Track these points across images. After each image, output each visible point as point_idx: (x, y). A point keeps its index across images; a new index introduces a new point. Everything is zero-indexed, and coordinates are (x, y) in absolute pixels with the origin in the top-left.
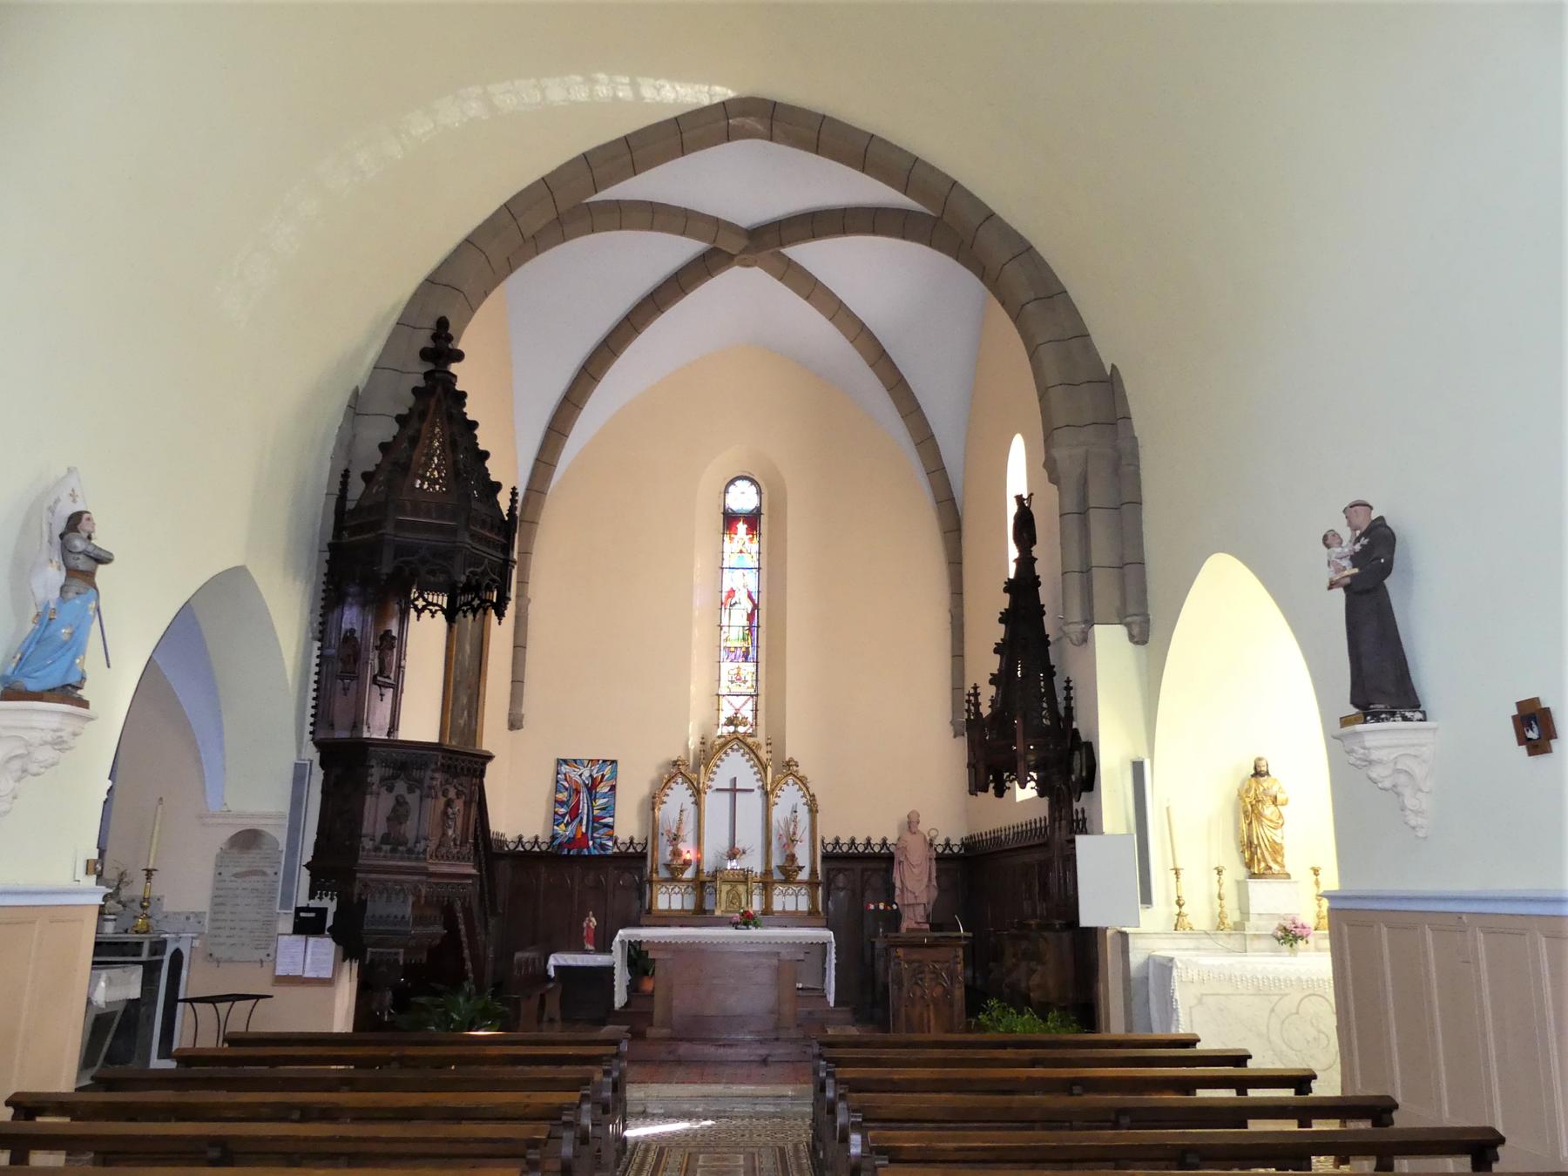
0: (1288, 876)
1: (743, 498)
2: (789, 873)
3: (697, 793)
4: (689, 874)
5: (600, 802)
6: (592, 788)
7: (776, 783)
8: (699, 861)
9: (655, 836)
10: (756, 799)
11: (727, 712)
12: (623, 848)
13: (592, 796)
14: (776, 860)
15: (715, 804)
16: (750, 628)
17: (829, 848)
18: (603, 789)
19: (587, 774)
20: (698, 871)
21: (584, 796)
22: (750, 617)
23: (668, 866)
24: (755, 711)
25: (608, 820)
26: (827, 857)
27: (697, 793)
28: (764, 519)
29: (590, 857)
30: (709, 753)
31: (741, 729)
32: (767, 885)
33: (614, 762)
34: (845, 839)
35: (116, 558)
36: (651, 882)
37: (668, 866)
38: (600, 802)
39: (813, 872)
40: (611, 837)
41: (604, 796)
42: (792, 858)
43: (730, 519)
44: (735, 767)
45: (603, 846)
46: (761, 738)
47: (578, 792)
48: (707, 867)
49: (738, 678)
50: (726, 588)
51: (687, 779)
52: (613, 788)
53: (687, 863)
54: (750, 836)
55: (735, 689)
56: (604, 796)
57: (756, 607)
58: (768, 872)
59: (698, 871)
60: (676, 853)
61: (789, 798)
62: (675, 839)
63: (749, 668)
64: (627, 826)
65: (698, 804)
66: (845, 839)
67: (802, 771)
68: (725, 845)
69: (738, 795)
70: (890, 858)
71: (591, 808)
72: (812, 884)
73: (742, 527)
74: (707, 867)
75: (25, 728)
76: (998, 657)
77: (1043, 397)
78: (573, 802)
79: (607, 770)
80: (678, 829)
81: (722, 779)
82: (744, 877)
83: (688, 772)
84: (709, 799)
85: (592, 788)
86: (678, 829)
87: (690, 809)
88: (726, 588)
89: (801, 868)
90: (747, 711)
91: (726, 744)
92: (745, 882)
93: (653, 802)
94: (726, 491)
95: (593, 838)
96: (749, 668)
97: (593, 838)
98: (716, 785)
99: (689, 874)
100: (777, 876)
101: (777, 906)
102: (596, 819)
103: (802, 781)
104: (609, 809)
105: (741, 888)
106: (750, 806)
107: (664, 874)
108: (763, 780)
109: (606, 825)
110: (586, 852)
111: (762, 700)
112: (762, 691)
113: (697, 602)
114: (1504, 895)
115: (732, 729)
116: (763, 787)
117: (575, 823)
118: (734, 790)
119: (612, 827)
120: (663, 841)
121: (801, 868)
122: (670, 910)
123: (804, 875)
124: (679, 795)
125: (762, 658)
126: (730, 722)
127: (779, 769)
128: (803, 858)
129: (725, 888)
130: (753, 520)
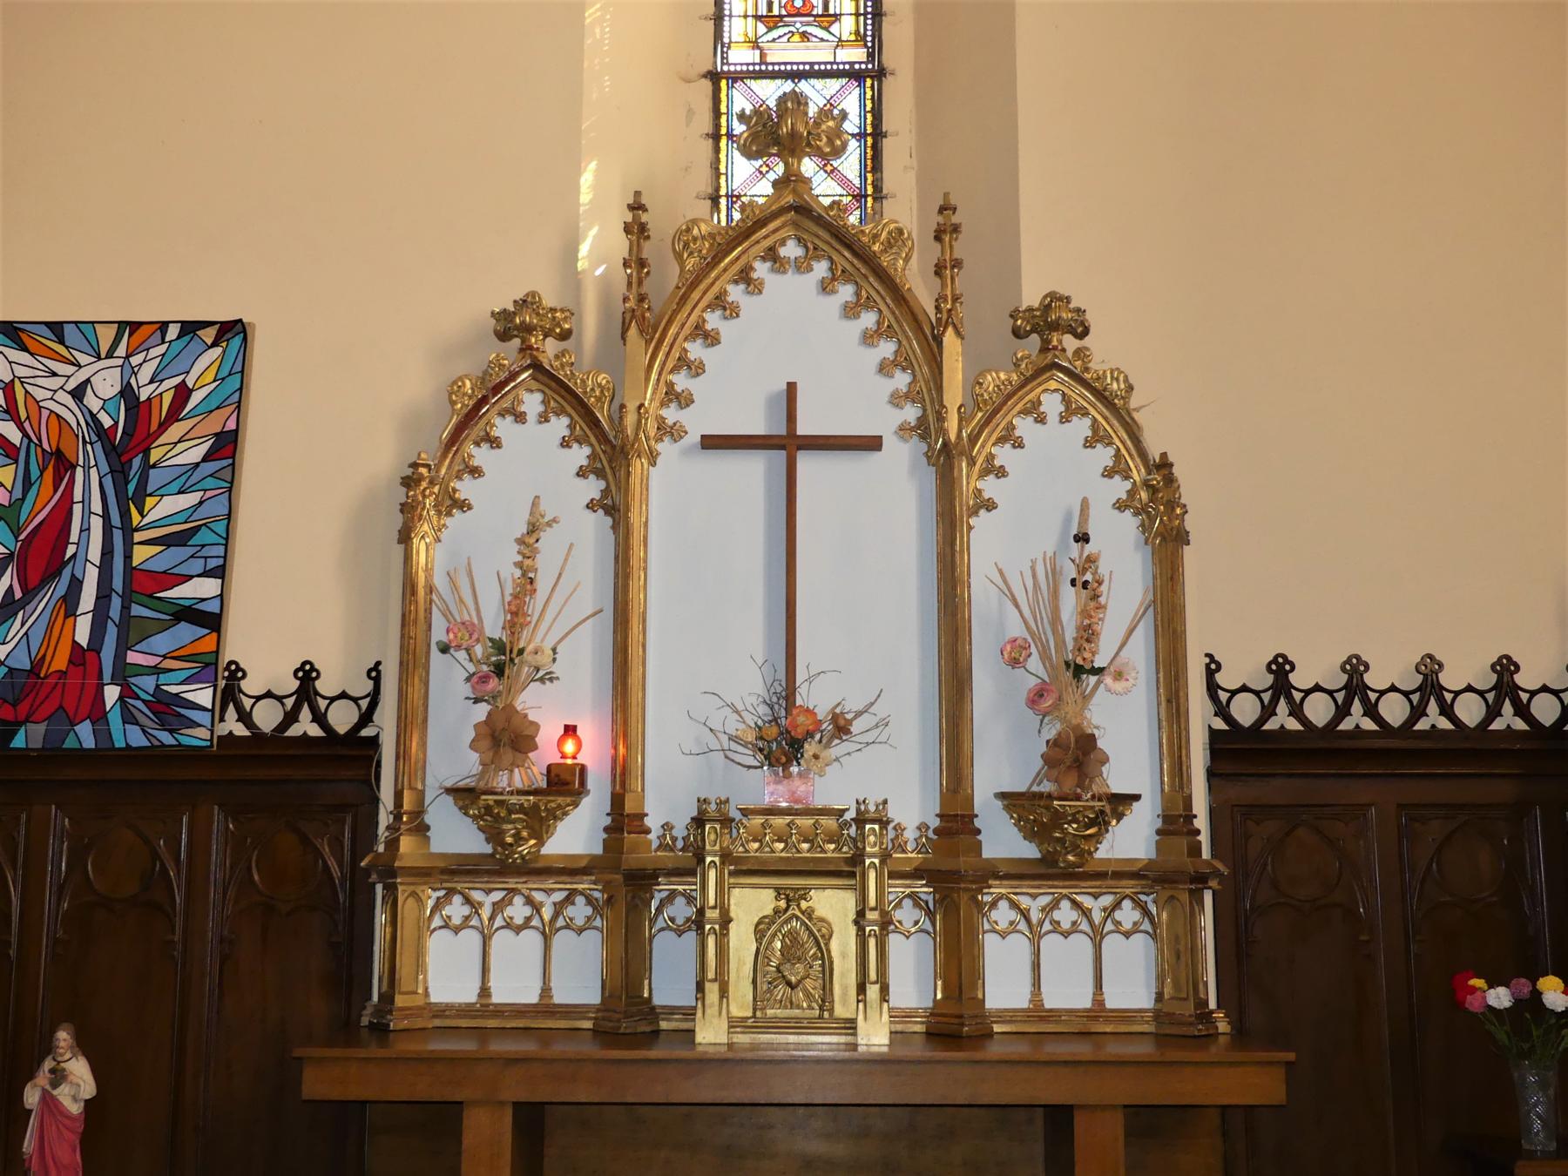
0: (378, 663)
2: (1068, 804)
3: (612, 454)
4: (576, 834)
5: (165, 507)
6: (129, 442)
7: (991, 412)
8: (623, 776)
9: (413, 661)
10: (896, 483)
12: (267, 717)
13: (129, 489)
14: (1005, 760)
15: (698, 507)
17: (1245, 711)
18: (181, 449)
19: (107, 383)
20: (623, 819)
21: (90, 483)
23: (464, 795)
25: (202, 589)
26: (1231, 748)
27: (612, 454)
29: (105, 755)
30: (679, 280)
32: (951, 877)
33: (232, 330)
34: (1316, 668)
36: (389, 873)
37: (464, 795)
38: (165, 507)
39: (1175, 823)
40: (207, 666)
41: (185, 480)
42: (1076, 754)
44: (794, 338)
45: (168, 709)
47: (62, 464)
48: (665, 807)
51: (564, 395)
52: (226, 446)
53: (565, 784)
54: (869, 654)
56: (185, 480)
58: (956, 823)
59: (623, 819)
60: (506, 736)
61: (1048, 476)
62: (503, 664)
64: (290, 616)
65: (614, 507)
66: (1316, 668)
67: (1105, 350)
68: (747, 688)
69: (807, 464)
70: (355, 753)
71: (120, 530)
72: (1162, 879)
74: (665, 807)
75: (1017, 606)
78: (37, 510)
79: (204, 366)
80: (516, 615)
81: (730, 391)
82: (843, 850)
83: (568, 381)
84: (670, 483)
85: (129, 442)
86: (516, 615)
87: (580, 538)
89: (1122, 802)
91: (731, 250)
92: (848, 871)
93: (424, 492)
95: (123, 674)
97: (123, 674)
98: (697, 422)
99: (576, 834)
100: (1002, 840)
101: (1004, 986)
102: (145, 584)
103: (1110, 406)
104: (207, 541)
105: (832, 904)
106: (870, 514)
107: (455, 834)
108: (928, 392)
109: (189, 614)
110: (85, 735)
114: (634, 651)
116: (923, 429)
117: (44, 603)
118: (788, 444)
119: (212, 621)
120: (449, 680)
121: (1122, 802)
122: (484, 1007)
123: (1131, 840)
124: (533, 459)
127: (980, 349)
128: (1130, 763)
129: (751, 903)
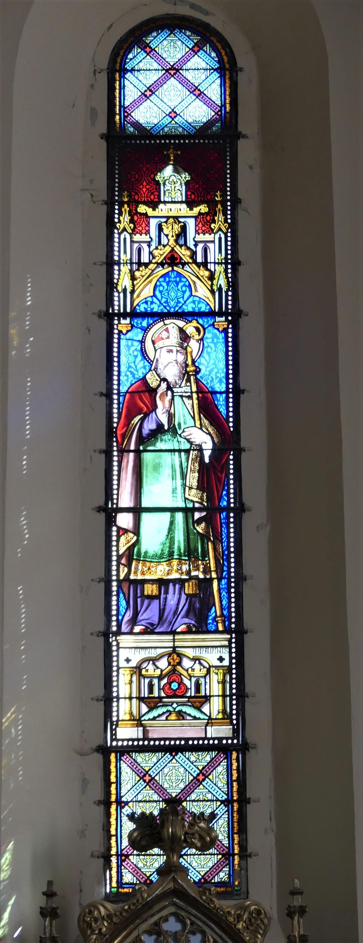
1: (173, 91)
11: (136, 796)
16: (212, 511)
22: (210, 475)
24: (239, 801)
28: (248, 152)
31: (198, 864)
35: (41, 893)
43: (133, 159)
46: (264, 892)
49: (172, 691)
50: (125, 382)
55: (167, 729)
57: (228, 441)
63: (211, 652)
73: (172, 181)
76: (165, 930)
77: (246, 838)
88: (125, 382)
90: (209, 798)
94: (116, 69)
96: (211, 652)
111: (261, 763)
112: (260, 731)
113: (26, 424)
115: (151, 862)
125: (257, 617)
126: (148, 833)
130: (206, 156)
